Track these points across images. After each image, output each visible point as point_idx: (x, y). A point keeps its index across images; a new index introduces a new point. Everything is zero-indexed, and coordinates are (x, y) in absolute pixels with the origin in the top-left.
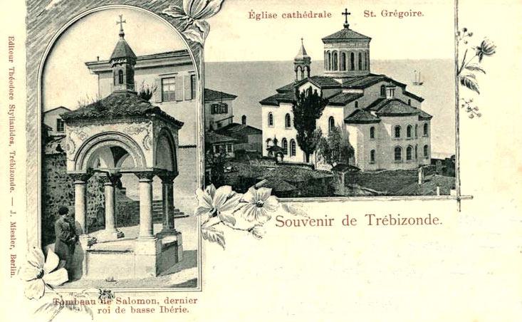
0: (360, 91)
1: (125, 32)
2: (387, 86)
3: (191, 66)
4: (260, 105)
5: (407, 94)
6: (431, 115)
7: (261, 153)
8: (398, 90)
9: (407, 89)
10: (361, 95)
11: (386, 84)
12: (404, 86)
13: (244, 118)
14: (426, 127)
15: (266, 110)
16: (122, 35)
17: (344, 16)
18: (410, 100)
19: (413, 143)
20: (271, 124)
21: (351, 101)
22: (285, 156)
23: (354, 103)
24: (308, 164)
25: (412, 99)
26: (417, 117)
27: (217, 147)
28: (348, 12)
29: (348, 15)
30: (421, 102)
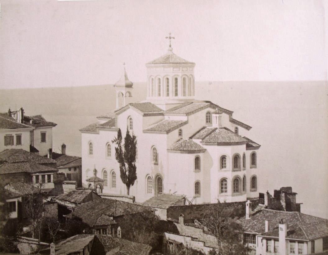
0: (184, 118)
1: (172, 45)
2: (213, 113)
3: (174, 94)
4: (80, 132)
5: (233, 121)
6: (56, 123)
7: (264, 230)
8: (225, 116)
9: (234, 117)
10: (186, 123)
11: (212, 110)
12: (230, 113)
13: (64, 147)
14: (253, 156)
15: (86, 137)
16: (170, 46)
17: (168, 40)
18: (237, 128)
19: (241, 174)
20: (91, 153)
21: (175, 128)
22: (104, 187)
23: (176, 132)
24: (129, 197)
25: (240, 128)
26: (245, 146)
27: (37, 177)
28: (172, 36)
29: (172, 39)
30: (249, 130)
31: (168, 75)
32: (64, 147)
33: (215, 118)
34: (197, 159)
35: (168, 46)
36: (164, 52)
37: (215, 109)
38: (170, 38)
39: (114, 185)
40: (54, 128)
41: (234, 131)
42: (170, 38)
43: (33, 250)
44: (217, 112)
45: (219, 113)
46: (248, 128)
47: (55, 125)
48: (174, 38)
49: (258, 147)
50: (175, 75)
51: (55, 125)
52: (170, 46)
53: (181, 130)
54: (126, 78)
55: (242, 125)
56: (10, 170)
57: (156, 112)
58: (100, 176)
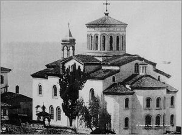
1: (108, 10)
5: (157, 71)
8: (150, 67)
9: (157, 67)
12: (154, 65)
13: (17, 88)
14: (172, 98)
16: (107, 11)
19: (162, 112)
20: (40, 93)
23: (111, 77)
24: (71, 127)
31: (97, 34)
32: (17, 88)
33: (142, 68)
34: (127, 100)
35: (106, 10)
36: (101, 15)
37: (142, 61)
38: (107, 4)
39: (59, 118)
40: (8, 74)
41: (157, 79)
42: (107, 4)
43: (140, 120)
44: (144, 63)
45: (145, 65)
46: (168, 76)
47: (10, 70)
48: (104, 4)
49: (176, 92)
50: (104, 34)
51: (10, 70)
52: (107, 11)
53: (114, 77)
54: (70, 35)
55: (163, 73)
56: (151, 74)
57: (94, 62)
58: (47, 111)
